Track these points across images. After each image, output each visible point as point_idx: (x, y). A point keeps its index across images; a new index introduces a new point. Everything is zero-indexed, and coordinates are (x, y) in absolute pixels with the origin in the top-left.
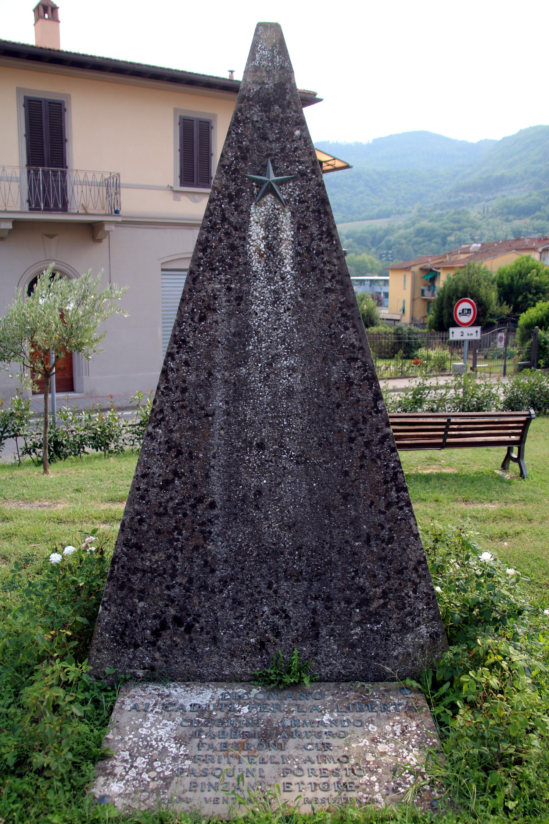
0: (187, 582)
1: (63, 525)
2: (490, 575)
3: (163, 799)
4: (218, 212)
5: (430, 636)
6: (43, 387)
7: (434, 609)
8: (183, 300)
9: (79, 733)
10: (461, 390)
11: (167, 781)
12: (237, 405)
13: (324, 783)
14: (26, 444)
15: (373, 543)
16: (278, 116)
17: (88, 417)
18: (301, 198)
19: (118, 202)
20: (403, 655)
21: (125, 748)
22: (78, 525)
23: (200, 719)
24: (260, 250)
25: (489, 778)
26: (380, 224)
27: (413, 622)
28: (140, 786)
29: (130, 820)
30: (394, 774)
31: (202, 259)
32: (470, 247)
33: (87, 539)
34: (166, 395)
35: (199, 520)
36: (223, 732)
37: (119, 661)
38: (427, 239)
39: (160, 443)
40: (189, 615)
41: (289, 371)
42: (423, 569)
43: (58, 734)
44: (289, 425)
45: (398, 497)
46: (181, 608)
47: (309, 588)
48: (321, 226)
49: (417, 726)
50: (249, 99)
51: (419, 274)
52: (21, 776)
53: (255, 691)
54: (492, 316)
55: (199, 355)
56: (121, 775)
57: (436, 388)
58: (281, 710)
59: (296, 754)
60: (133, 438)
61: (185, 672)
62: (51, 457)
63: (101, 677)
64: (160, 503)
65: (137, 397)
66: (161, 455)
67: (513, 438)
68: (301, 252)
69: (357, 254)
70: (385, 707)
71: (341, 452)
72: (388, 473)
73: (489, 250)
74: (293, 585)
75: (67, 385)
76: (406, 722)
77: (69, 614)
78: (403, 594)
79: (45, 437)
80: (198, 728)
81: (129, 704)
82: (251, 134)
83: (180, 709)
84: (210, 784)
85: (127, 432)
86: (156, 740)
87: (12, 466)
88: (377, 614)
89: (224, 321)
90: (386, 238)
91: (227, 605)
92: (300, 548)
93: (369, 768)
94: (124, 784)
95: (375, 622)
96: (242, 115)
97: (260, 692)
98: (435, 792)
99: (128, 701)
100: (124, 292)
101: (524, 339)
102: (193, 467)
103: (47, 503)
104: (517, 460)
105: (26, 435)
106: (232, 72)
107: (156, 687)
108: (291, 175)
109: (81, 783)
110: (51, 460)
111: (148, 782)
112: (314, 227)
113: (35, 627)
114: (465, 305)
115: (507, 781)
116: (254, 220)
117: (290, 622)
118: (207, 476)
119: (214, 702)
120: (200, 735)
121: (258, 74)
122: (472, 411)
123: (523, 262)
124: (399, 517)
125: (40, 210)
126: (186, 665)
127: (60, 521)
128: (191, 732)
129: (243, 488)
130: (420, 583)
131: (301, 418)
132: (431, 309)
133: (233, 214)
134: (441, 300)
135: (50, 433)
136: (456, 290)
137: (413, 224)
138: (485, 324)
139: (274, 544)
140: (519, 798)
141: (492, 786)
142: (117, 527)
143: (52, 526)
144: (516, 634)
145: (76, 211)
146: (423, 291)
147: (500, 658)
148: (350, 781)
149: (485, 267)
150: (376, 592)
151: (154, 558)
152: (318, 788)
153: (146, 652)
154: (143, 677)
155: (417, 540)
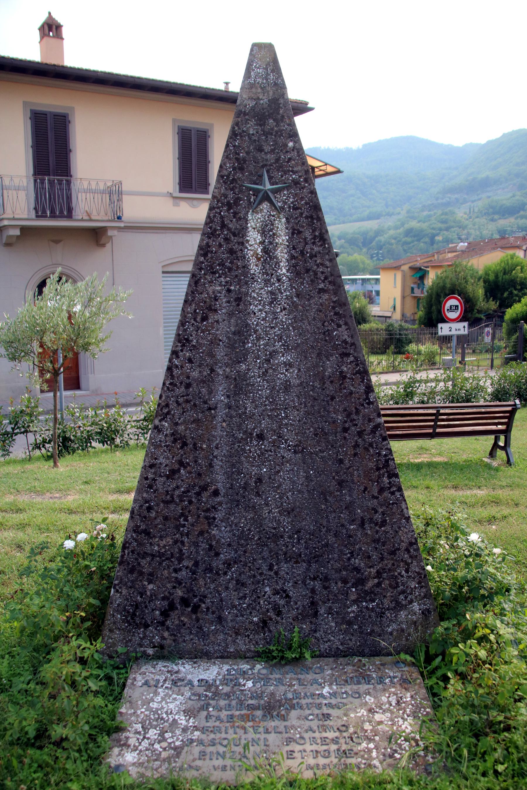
0: (193, 565)
1: (74, 515)
2: (478, 555)
3: (174, 767)
4: (218, 220)
5: (422, 612)
6: (52, 385)
7: (426, 587)
8: (186, 301)
9: (94, 707)
10: (451, 383)
11: (178, 750)
12: (238, 399)
13: (325, 751)
14: (36, 440)
15: (367, 526)
16: (272, 129)
17: (94, 413)
18: (295, 205)
19: (121, 209)
20: (397, 630)
21: (137, 720)
22: (87, 515)
23: (208, 693)
24: (258, 254)
25: (480, 744)
26: (372, 225)
27: (406, 600)
28: (152, 756)
29: (144, 786)
30: (390, 742)
31: (203, 263)
32: (457, 246)
33: (98, 527)
34: (172, 391)
35: (203, 507)
36: (230, 705)
37: (130, 641)
38: (416, 238)
39: (166, 435)
40: (195, 596)
41: (286, 366)
42: (415, 550)
43: (75, 709)
44: (286, 417)
45: (390, 483)
46: (187, 590)
47: (308, 569)
48: (314, 231)
49: (412, 697)
50: (245, 114)
51: (409, 273)
52: (41, 748)
53: (258, 667)
54: (479, 312)
55: (202, 353)
56: (134, 746)
57: (426, 382)
58: (283, 684)
59: (298, 724)
60: (137, 433)
61: (193, 650)
62: (60, 452)
63: (114, 655)
64: (167, 491)
65: (140, 394)
66: (167, 446)
67: (500, 427)
68: (296, 255)
69: (349, 255)
70: (381, 681)
71: (336, 442)
72: (380, 460)
73: (476, 248)
74: (293, 566)
75: (74, 383)
76: (401, 693)
77: (82, 597)
78: (396, 574)
79: (55, 433)
80: (206, 702)
81: (140, 680)
82: (247, 145)
83: (188, 684)
84: (218, 753)
85: (132, 427)
86: (166, 713)
87: (23, 461)
88: (372, 592)
89: (224, 320)
90: (377, 239)
91: (231, 586)
92: (298, 532)
93: (367, 736)
94: (138, 754)
95: (370, 600)
96: (239, 129)
97: (263, 668)
98: (429, 758)
99: (139, 677)
100: (129, 295)
101: (510, 333)
102: (197, 457)
103: (57, 495)
104: (505, 448)
105: (36, 431)
106: (227, 84)
107: (165, 664)
108: (285, 183)
109: (97, 754)
110: (61, 454)
111: (160, 752)
112: (307, 232)
113: (51, 608)
114: (453, 302)
115: (496, 746)
116: (251, 226)
117: (290, 602)
118: (211, 466)
119: (220, 677)
120: (207, 708)
121: (254, 90)
122: (461, 402)
123: (508, 260)
124: (391, 502)
125: (46, 217)
126: (193, 643)
127: (71, 512)
128: (199, 706)
129: (245, 477)
130: (412, 563)
131: (298, 410)
132: (421, 305)
133: (231, 221)
134: (430, 296)
135: (59, 429)
136: (444, 287)
137: (403, 224)
138: (472, 319)
139: (275, 529)
140: (509, 762)
141: (482, 751)
142: (127, 516)
143: (63, 516)
144: (503, 609)
145: (80, 218)
146: (412, 289)
147: (488, 631)
148: (349, 748)
149: (472, 265)
150: (370, 572)
151: (162, 543)
152: (319, 755)
153: (156, 632)
154: (153, 655)
155: (408, 522)
